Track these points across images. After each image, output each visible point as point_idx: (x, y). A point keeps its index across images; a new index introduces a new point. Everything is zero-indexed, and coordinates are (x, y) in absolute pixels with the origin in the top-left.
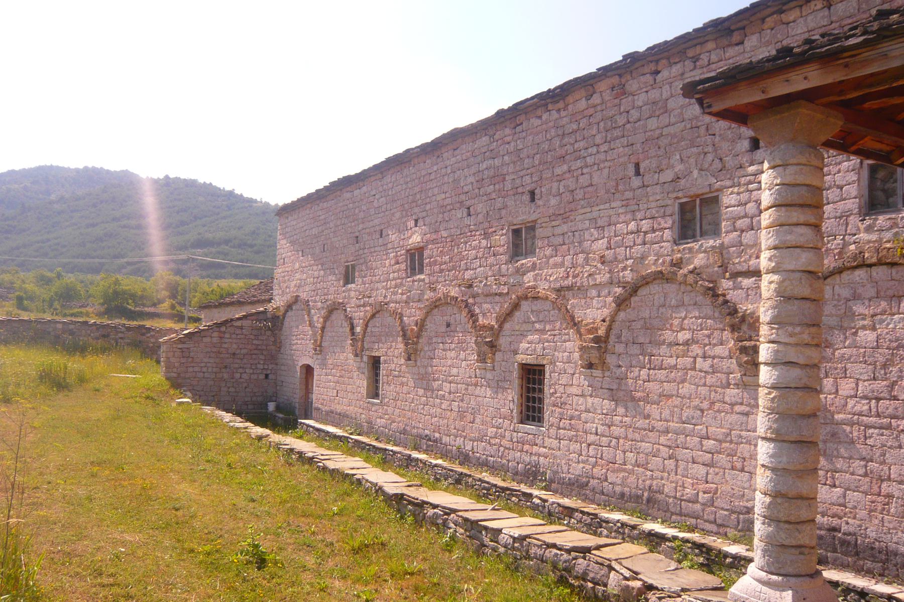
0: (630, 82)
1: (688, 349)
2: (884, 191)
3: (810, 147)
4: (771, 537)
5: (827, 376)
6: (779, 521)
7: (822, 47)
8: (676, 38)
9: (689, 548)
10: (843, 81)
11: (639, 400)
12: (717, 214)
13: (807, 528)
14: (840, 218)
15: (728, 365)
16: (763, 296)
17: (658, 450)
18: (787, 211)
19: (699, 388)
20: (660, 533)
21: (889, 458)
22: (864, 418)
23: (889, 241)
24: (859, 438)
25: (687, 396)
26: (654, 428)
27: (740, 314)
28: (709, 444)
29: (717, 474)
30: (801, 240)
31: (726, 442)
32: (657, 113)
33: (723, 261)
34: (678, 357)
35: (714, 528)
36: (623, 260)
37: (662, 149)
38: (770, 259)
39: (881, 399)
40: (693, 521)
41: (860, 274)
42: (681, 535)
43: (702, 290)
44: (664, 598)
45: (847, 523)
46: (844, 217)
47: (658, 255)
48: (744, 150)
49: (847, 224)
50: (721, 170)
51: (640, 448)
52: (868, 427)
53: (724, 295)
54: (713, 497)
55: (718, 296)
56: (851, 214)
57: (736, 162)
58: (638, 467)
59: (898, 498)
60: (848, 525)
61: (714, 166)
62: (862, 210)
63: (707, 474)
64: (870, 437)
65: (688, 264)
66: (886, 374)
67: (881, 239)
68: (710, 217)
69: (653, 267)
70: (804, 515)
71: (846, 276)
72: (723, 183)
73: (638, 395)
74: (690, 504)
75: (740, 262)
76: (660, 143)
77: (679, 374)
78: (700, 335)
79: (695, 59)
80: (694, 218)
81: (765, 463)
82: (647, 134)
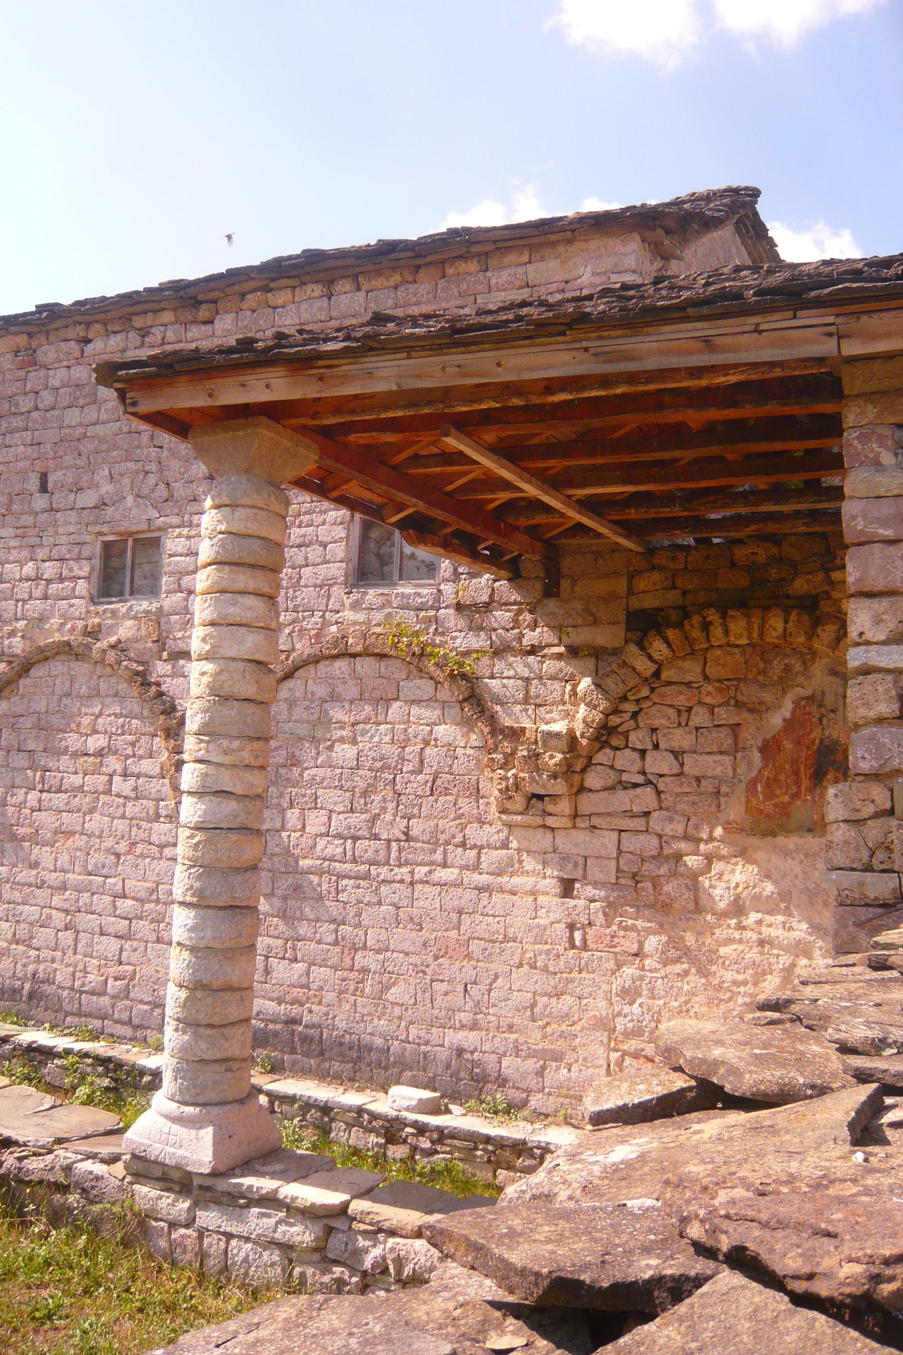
0: (44, 348)
1: (101, 761)
2: (378, 556)
3: (271, 484)
4: (186, 1052)
5: (291, 806)
6: (199, 1025)
7: (291, 347)
8: (118, 296)
9: (88, 1065)
10: (319, 399)
11: (23, 839)
12: (156, 565)
13: (237, 1032)
14: (321, 586)
15: (158, 787)
16: (192, 693)
17: (49, 917)
18: (231, 571)
19: (115, 821)
20: (45, 1046)
21: (366, 920)
22: (337, 864)
23: (378, 625)
24: (329, 893)
25: (97, 833)
26: (43, 882)
27: (179, 714)
28: (126, 905)
29: (136, 950)
30: (249, 616)
31: (151, 901)
32: (82, 402)
33: (160, 634)
34: (86, 774)
35: (127, 1031)
36: (11, 621)
37: (84, 458)
38: (204, 640)
39: (359, 838)
40: (97, 1023)
41: (341, 665)
42: (78, 1046)
43: (126, 674)
44: (26, 1157)
45: (310, 1011)
46: (325, 585)
47: (66, 618)
48: (200, 475)
49: (329, 596)
50: (166, 501)
51: (21, 914)
52: (341, 876)
53: (158, 684)
54: (128, 985)
55: (149, 684)
56: (335, 583)
57: (189, 491)
58: (17, 943)
59: (375, 973)
60: (311, 1014)
61: (157, 494)
62: (350, 579)
63: (121, 950)
64: (343, 891)
65: (109, 634)
66: (366, 804)
67: (370, 621)
68: (146, 567)
69: (57, 634)
70: (234, 1013)
71: (322, 667)
72: (168, 520)
73: (22, 831)
74: (95, 998)
75: (183, 637)
76: (81, 447)
77: (87, 800)
78: (120, 742)
79: (144, 333)
80: (124, 567)
81: (181, 940)
82: (64, 431)
